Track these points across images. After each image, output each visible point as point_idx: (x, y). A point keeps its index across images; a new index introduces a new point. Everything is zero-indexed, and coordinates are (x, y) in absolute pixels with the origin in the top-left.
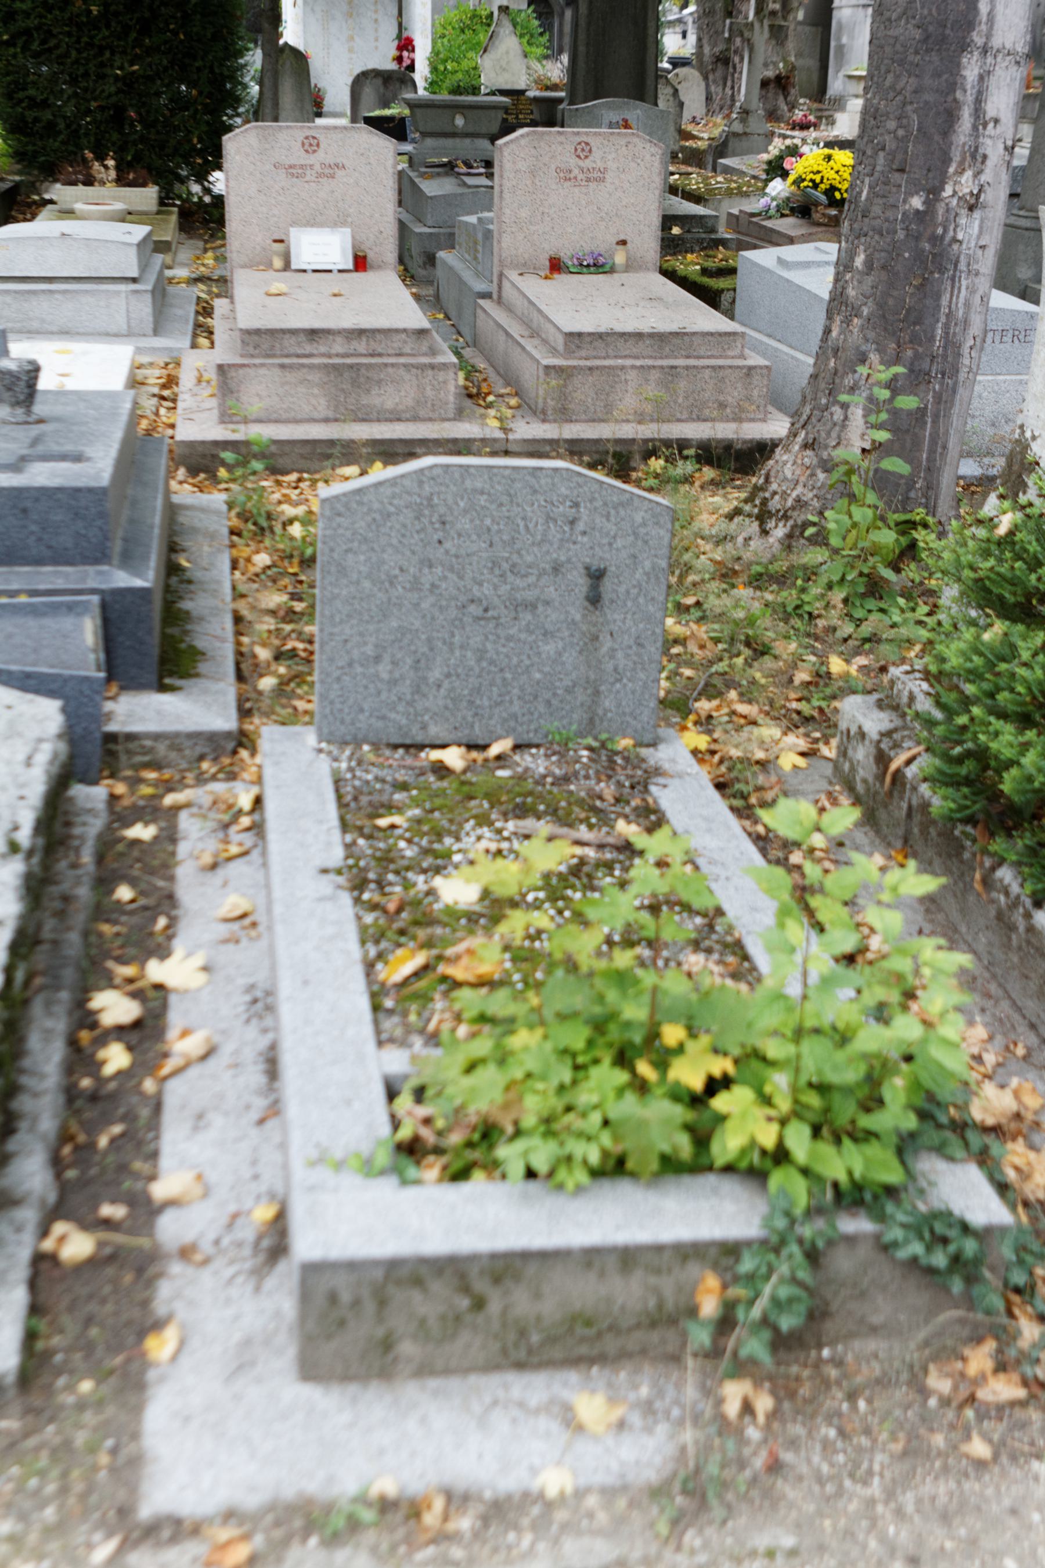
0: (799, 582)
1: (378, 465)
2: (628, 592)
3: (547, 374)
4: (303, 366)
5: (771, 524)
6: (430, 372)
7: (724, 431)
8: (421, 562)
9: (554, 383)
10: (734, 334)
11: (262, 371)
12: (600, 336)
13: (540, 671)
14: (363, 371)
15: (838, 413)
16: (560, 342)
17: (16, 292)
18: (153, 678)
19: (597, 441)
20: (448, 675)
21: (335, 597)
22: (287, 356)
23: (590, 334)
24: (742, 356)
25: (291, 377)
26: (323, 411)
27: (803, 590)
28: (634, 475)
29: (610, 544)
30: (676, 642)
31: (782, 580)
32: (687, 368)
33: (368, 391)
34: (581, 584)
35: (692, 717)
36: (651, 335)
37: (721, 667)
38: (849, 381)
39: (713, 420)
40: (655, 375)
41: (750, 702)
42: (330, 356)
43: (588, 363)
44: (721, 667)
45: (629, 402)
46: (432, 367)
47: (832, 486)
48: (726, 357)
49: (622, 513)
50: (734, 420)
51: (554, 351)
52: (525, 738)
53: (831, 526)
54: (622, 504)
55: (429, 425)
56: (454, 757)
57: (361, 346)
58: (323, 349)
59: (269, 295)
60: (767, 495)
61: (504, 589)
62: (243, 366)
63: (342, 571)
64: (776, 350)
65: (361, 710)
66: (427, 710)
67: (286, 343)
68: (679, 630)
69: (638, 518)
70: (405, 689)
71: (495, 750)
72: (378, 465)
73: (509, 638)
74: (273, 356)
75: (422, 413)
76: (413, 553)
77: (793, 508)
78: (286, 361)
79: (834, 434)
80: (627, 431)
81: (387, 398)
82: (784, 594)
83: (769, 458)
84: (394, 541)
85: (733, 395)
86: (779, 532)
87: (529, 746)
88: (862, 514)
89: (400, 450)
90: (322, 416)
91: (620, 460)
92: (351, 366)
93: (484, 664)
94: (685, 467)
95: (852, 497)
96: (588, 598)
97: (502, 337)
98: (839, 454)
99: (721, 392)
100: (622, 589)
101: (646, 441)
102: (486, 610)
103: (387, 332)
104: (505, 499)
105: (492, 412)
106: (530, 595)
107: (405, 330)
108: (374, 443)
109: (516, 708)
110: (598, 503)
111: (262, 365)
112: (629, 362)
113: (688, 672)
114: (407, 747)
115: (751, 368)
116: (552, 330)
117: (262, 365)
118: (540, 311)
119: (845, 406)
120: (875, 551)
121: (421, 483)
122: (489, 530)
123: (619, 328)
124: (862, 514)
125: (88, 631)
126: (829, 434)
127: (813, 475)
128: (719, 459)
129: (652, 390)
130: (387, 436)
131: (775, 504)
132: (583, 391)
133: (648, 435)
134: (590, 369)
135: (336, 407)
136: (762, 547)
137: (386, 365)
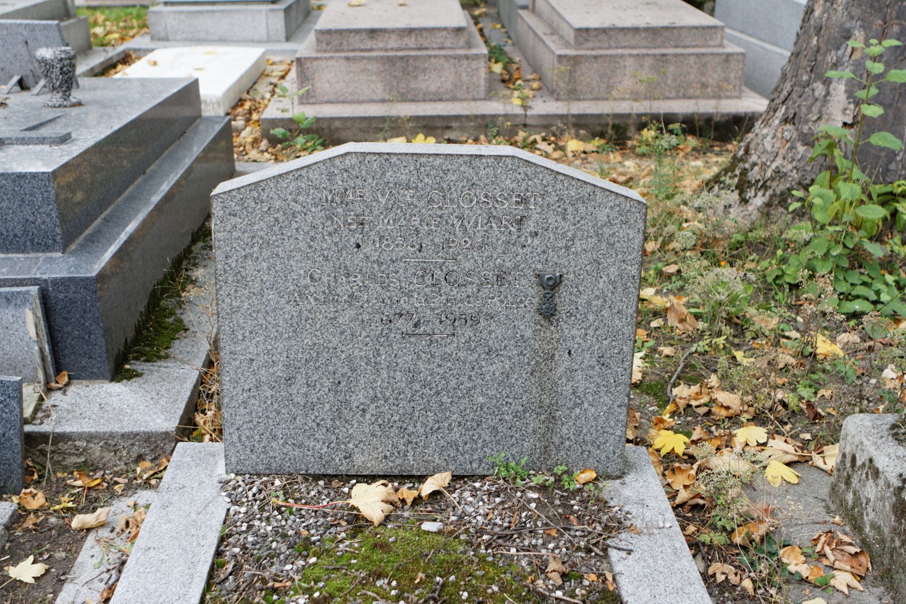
0: (779, 252)
1: (421, 136)
2: (589, 303)
3: (560, 62)
4: (364, 58)
5: (750, 193)
6: (465, 62)
7: (705, 106)
8: (337, 269)
9: (563, 68)
10: (715, 27)
11: (331, 63)
12: (604, 31)
13: (482, 394)
14: (411, 61)
15: (819, 89)
16: (570, 36)
17: (188, 12)
18: (107, 368)
19: (599, 116)
20: (374, 399)
21: (235, 311)
22: (353, 51)
23: (596, 29)
24: (721, 45)
25: (354, 67)
26: (380, 94)
27: (784, 260)
28: (630, 143)
29: (567, 248)
30: (656, 314)
31: (761, 247)
32: (675, 55)
33: (416, 77)
34: (533, 294)
35: (670, 408)
36: (647, 30)
37: (702, 346)
38: (831, 57)
39: (696, 98)
40: (648, 62)
41: (732, 389)
42: (386, 50)
43: (594, 53)
44: (702, 346)
45: (626, 83)
46: (467, 57)
47: (812, 159)
48: (708, 46)
49: (582, 210)
50: (714, 97)
51: (567, 44)
52: (468, 469)
53: (817, 201)
54: (581, 199)
55: (465, 104)
56: (370, 500)
57: (411, 42)
58: (381, 45)
59: (350, 5)
60: (747, 166)
61: (437, 302)
62: (316, 59)
63: (241, 280)
64: (748, 42)
65: (275, 438)
66: (351, 437)
67: (351, 40)
68: (659, 302)
69: (602, 216)
70: (325, 412)
71: (427, 488)
72: (421, 136)
73: (445, 357)
74: (342, 51)
75: (459, 95)
76: (326, 259)
77: (772, 179)
78: (351, 54)
79: (815, 109)
80: (624, 107)
81: (431, 82)
82: (765, 263)
83: (748, 131)
84: (303, 245)
85: (713, 77)
86: (759, 201)
87: (473, 477)
88: (848, 190)
89: (439, 124)
90: (379, 98)
91: (616, 133)
92: (402, 58)
93: (416, 386)
94: (668, 140)
95: (834, 170)
96: (539, 311)
97: (531, 36)
98: (822, 127)
99: (703, 74)
100: (582, 300)
101: (640, 116)
102: (416, 325)
103: (432, 30)
104: (436, 195)
105: (516, 93)
106: (469, 308)
107: (445, 29)
108: (417, 118)
109: (455, 435)
110: (552, 199)
111: (332, 58)
112: (627, 52)
113: (667, 351)
114: (329, 478)
115: (728, 55)
116: (566, 27)
117: (332, 58)
118: (559, 14)
119: (827, 82)
120: (858, 226)
121: (331, 176)
122: (417, 231)
123: (620, 24)
124: (848, 190)
125: (29, 323)
126: (809, 109)
127: (792, 148)
128: (701, 130)
129: (645, 74)
130: (429, 113)
131: (755, 174)
132: (589, 75)
133: (642, 110)
134: (595, 57)
135: (391, 90)
136: (739, 216)
137: (430, 56)
